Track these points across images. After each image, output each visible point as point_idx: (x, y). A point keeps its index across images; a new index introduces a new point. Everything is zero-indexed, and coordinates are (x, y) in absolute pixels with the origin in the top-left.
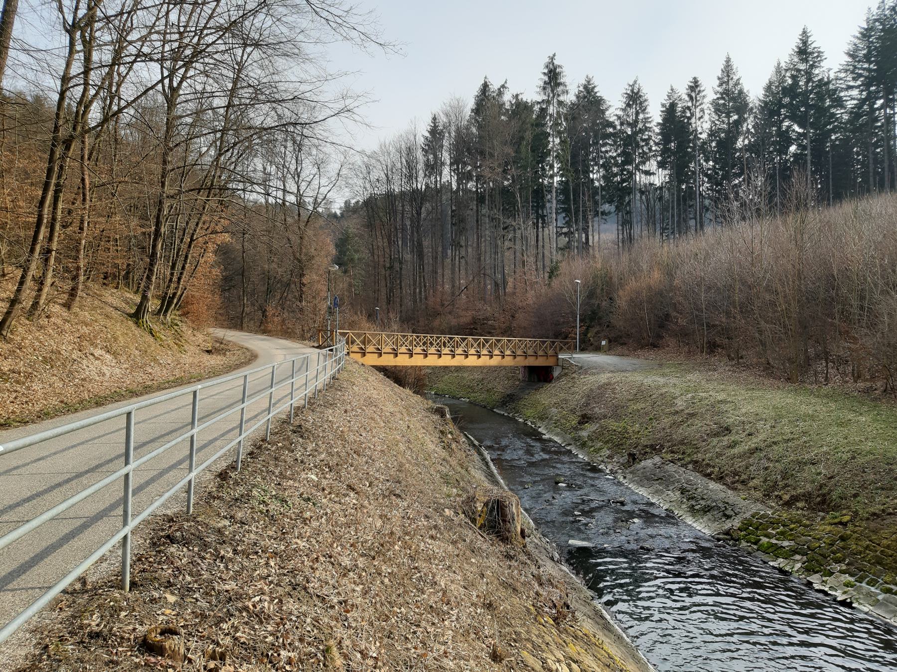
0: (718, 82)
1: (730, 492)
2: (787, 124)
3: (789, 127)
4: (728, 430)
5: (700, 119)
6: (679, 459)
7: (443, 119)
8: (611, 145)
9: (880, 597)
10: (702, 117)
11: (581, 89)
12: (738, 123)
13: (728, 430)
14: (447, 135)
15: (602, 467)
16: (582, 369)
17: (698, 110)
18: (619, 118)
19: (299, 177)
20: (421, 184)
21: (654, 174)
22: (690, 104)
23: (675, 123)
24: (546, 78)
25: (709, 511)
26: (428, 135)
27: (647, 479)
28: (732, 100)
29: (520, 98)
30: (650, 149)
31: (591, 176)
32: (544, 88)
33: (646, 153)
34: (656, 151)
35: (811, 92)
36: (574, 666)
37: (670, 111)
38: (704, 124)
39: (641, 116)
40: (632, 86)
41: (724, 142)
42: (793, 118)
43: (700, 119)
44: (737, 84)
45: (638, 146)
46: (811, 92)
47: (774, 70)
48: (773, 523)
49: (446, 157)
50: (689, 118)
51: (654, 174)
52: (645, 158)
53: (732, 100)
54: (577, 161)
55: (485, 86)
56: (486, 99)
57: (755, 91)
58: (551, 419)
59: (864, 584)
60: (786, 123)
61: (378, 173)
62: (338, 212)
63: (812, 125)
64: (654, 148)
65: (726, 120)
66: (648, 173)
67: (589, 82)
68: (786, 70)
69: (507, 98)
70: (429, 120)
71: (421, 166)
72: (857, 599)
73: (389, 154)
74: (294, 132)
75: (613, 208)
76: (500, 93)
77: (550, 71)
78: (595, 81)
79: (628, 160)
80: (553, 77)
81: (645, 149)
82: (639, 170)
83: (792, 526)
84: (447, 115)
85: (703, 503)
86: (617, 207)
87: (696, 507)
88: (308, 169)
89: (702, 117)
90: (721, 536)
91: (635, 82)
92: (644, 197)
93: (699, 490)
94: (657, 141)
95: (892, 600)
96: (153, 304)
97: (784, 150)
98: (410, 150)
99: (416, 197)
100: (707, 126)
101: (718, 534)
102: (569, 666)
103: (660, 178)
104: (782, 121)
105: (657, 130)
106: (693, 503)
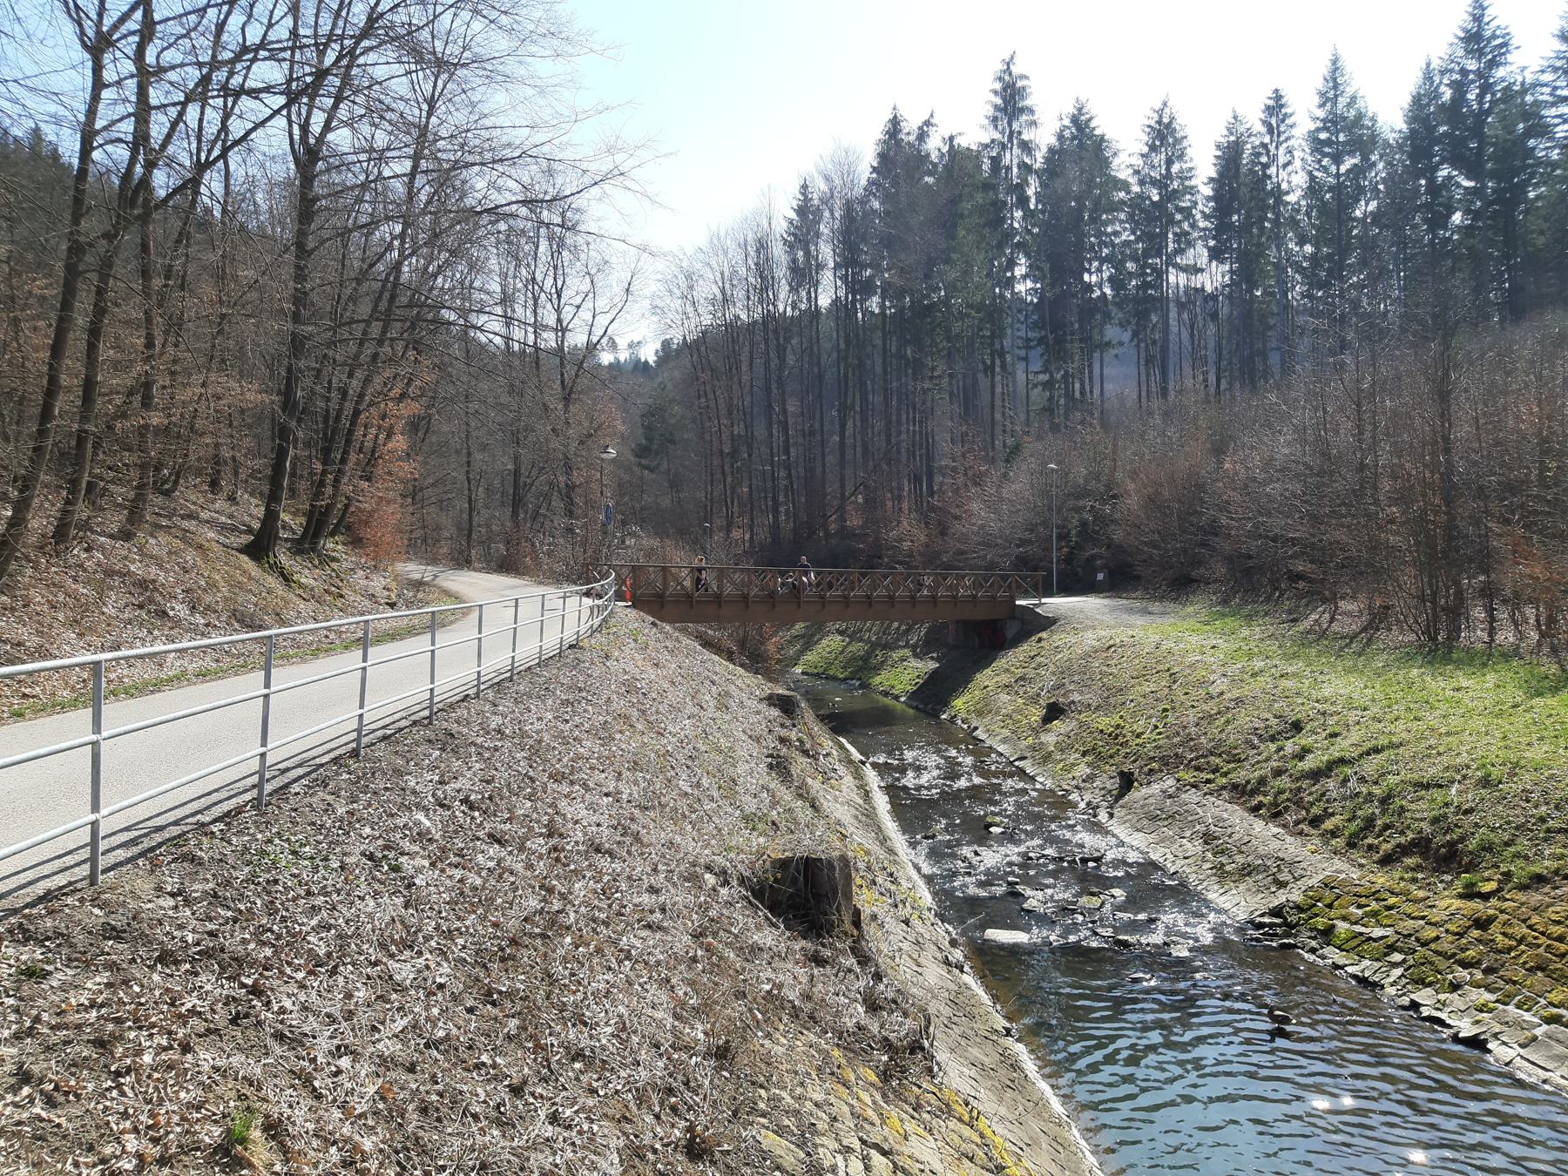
0: (1316, 100)
1: (1289, 839)
2: (1445, 173)
3: (1450, 178)
4: (1297, 727)
5: (1285, 166)
6: (1208, 781)
7: (819, 187)
8: (1122, 222)
9: (1538, 1032)
10: (1289, 163)
11: (1067, 122)
12: (1357, 172)
13: (1297, 727)
14: (827, 214)
15: (1074, 797)
16: (1048, 623)
17: (1282, 150)
18: (1137, 172)
19: (559, 297)
20: (784, 302)
21: (1202, 270)
22: (1267, 140)
23: (1242, 178)
24: (999, 101)
25: (1249, 874)
26: (793, 215)
27: (1152, 819)
28: (1344, 131)
29: (955, 143)
30: (1193, 226)
31: (1086, 277)
32: (995, 120)
33: (1188, 233)
34: (1204, 229)
35: (1488, 112)
36: (877, 1158)
37: (1230, 156)
38: (1292, 181)
39: (1175, 168)
40: (1160, 112)
41: (1332, 204)
42: (1456, 161)
43: (1285, 166)
44: (1353, 99)
45: (1172, 221)
46: (1488, 112)
47: (1420, 74)
48: (1359, 898)
49: (826, 252)
50: (1266, 166)
51: (1202, 270)
52: (1184, 241)
53: (1344, 131)
54: (1060, 252)
55: (895, 122)
56: (899, 155)
57: (1389, 114)
58: (998, 713)
59: (1511, 1008)
60: (1443, 172)
61: (707, 289)
62: (652, 360)
63: (1493, 175)
64: (1201, 224)
65: (1333, 169)
66: (1196, 270)
67: (1080, 110)
68: (1442, 73)
69: (934, 145)
70: (795, 190)
71: (781, 272)
72: (1495, 1036)
73: (726, 253)
74: (547, 221)
75: (1126, 337)
76: (922, 136)
77: (1005, 89)
78: (1092, 109)
79: (1155, 244)
80: (1011, 101)
81: (1186, 226)
82: (1176, 266)
83: (1392, 900)
84: (827, 178)
85: (1240, 859)
86: (1135, 334)
87: (1228, 868)
88: (575, 285)
89: (1289, 163)
90: (1266, 920)
91: (1165, 104)
92: (1185, 316)
93: (1236, 837)
94: (1207, 210)
95: (1560, 1036)
96: (291, 521)
97: (1439, 220)
98: (762, 245)
99: (772, 328)
100: (1300, 179)
101: (1262, 915)
102: (865, 1159)
103: (1215, 277)
104: (1436, 168)
105: (1207, 191)
106: (1224, 860)
